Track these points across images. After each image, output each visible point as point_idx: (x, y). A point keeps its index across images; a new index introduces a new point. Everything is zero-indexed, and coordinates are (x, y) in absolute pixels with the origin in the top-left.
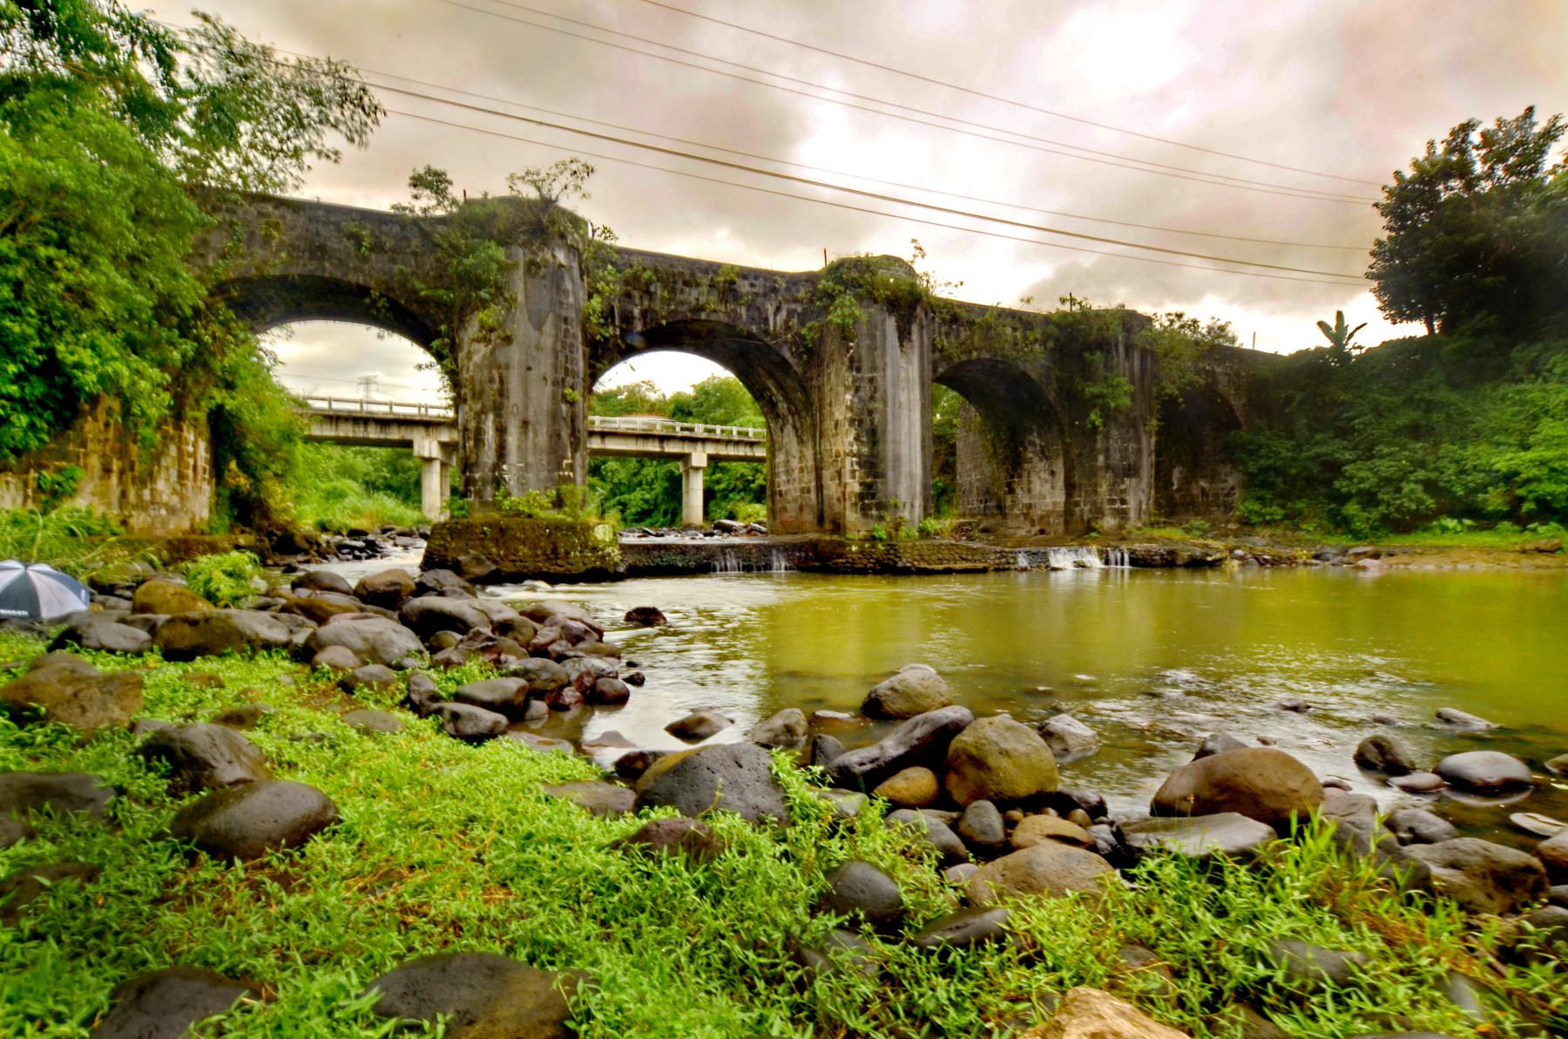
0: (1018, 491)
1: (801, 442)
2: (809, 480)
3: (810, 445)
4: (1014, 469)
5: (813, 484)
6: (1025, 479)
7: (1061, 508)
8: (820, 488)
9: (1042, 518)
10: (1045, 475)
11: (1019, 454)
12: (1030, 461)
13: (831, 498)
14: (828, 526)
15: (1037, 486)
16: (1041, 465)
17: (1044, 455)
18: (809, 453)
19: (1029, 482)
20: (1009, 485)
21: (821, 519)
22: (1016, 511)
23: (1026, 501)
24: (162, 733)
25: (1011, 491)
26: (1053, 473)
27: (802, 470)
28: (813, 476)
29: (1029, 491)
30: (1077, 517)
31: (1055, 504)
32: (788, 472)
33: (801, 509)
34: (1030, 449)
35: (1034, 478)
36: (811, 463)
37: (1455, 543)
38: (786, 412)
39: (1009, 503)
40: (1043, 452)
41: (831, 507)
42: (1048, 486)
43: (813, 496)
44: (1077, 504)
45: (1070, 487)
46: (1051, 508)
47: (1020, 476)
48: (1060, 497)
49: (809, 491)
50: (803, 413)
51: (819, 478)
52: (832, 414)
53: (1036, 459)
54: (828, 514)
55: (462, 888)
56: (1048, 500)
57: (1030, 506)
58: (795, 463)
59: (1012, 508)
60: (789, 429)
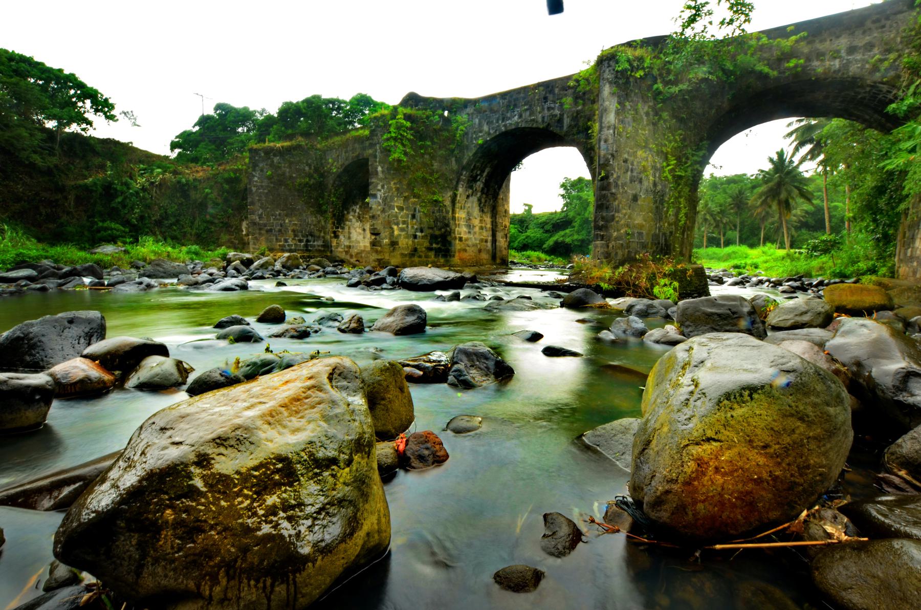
0: (341, 237)
1: (482, 211)
2: (487, 235)
4: (339, 223)
5: (490, 238)
6: (346, 230)
8: (494, 241)
9: (357, 254)
10: (360, 231)
11: (343, 215)
12: (350, 221)
13: (501, 247)
14: (498, 261)
15: (354, 236)
16: (358, 224)
17: (360, 218)
18: (488, 220)
19: (350, 233)
20: (334, 232)
21: (494, 257)
22: (340, 249)
23: (347, 243)
25: (336, 236)
26: (364, 230)
27: (481, 228)
28: (490, 233)
29: (349, 238)
33: (480, 251)
34: (352, 213)
35: (352, 231)
36: (489, 226)
38: (479, 189)
39: (334, 244)
40: (359, 217)
41: (501, 251)
42: (361, 237)
43: (489, 244)
47: (343, 228)
49: (486, 241)
50: (490, 197)
51: (494, 235)
53: (354, 220)
54: (498, 254)
55: (688, 363)
56: (362, 244)
57: (349, 247)
59: (337, 247)
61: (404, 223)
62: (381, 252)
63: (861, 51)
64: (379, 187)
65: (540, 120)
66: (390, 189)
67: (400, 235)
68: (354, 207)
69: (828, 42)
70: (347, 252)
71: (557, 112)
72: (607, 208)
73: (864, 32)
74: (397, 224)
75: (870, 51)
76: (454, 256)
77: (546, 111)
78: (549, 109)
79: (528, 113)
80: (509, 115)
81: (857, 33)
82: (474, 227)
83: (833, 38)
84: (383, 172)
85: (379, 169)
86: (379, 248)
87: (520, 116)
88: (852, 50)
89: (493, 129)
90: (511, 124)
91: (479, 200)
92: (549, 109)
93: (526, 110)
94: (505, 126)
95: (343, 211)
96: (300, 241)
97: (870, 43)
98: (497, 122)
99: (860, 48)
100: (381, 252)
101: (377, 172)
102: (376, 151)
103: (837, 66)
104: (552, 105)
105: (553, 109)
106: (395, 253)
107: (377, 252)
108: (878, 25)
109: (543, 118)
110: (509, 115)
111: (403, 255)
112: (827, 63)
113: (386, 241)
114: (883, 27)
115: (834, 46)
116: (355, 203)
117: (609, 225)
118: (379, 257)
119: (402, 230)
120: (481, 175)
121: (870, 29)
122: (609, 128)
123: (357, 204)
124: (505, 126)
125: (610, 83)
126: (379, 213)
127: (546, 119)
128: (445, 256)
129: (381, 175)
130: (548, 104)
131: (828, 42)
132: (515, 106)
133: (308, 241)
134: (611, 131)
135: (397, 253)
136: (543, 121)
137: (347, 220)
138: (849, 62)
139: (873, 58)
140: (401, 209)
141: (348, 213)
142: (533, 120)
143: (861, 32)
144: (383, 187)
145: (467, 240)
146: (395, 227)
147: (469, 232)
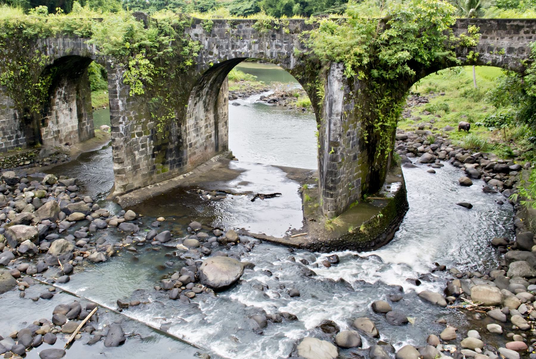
1: (207, 110)
3: (212, 111)
7: (76, 128)
10: (66, 112)
15: (62, 119)
16: (64, 106)
17: (66, 99)
18: (211, 116)
19: (57, 117)
22: (49, 137)
23: (55, 129)
24: (286, 4)
26: (71, 110)
29: (57, 122)
30: (84, 131)
31: (73, 127)
32: (197, 130)
33: (206, 148)
35: (60, 114)
37: (480, 114)
41: (222, 139)
42: (69, 118)
43: (213, 138)
44: (84, 124)
45: (80, 116)
46: (71, 130)
48: (75, 122)
52: (223, 95)
53: (60, 103)
56: (69, 126)
57: (58, 131)
58: (202, 124)
60: (201, 103)
61: (143, 146)
62: (125, 178)
63: (516, 52)
64: (121, 120)
65: (268, 54)
66: (130, 119)
67: (140, 158)
68: (60, 90)
69: (496, 40)
70: (56, 138)
71: (284, 51)
72: (336, 174)
73: (519, 39)
74: (138, 149)
75: (522, 54)
76: (186, 163)
77: (274, 48)
78: (277, 46)
79: (257, 46)
80: (238, 43)
81: (514, 38)
82: (201, 128)
83: (499, 38)
84: (123, 105)
85: (120, 103)
86: (124, 175)
87: (250, 47)
88: (510, 50)
89: (223, 53)
90: (241, 53)
91: (205, 102)
92: (277, 46)
93: (256, 43)
94: (235, 53)
95: (49, 96)
96: (10, 138)
97: (522, 47)
99: (516, 50)
100: (125, 178)
101: (118, 106)
102: (116, 86)
103: (501, 60)
104: (280, 44)
105: (281, 47)
106: (137, 176)
107: (122, 179)
108: (528, 35)
109: (272, 53)
111: (144, 175)
112: (494, 56)
113: (129, 167)
114: (531, 38)
115: (499, 45)
116: (61, 86)
117: (336, 186)
118: (124, 184)
119: (142, 153)
120: (207, 83)
121: (523, 37)
122: (337, 115)
123: (63, 85)
124: (235, 53)
125: (339, 81)
126: (122, 144)
127: (274, 55)
128: (179, 165)
129: (121, 109)
130: (276, 42)
131: (496, 40)
132: (244, 36)
133: (17, 137)
134: (339, 118)
135: (139, 175)
136: (272, 56)
137: (54, 105)
138: (508, 58)
139: (523, 59)
140: (140, 135)
141: (54, 97)
142: (262, 53)
143: (517, 38)
144: (124, 119)
145: (195, 143)
146: (136, 152)
147: (197, 135)
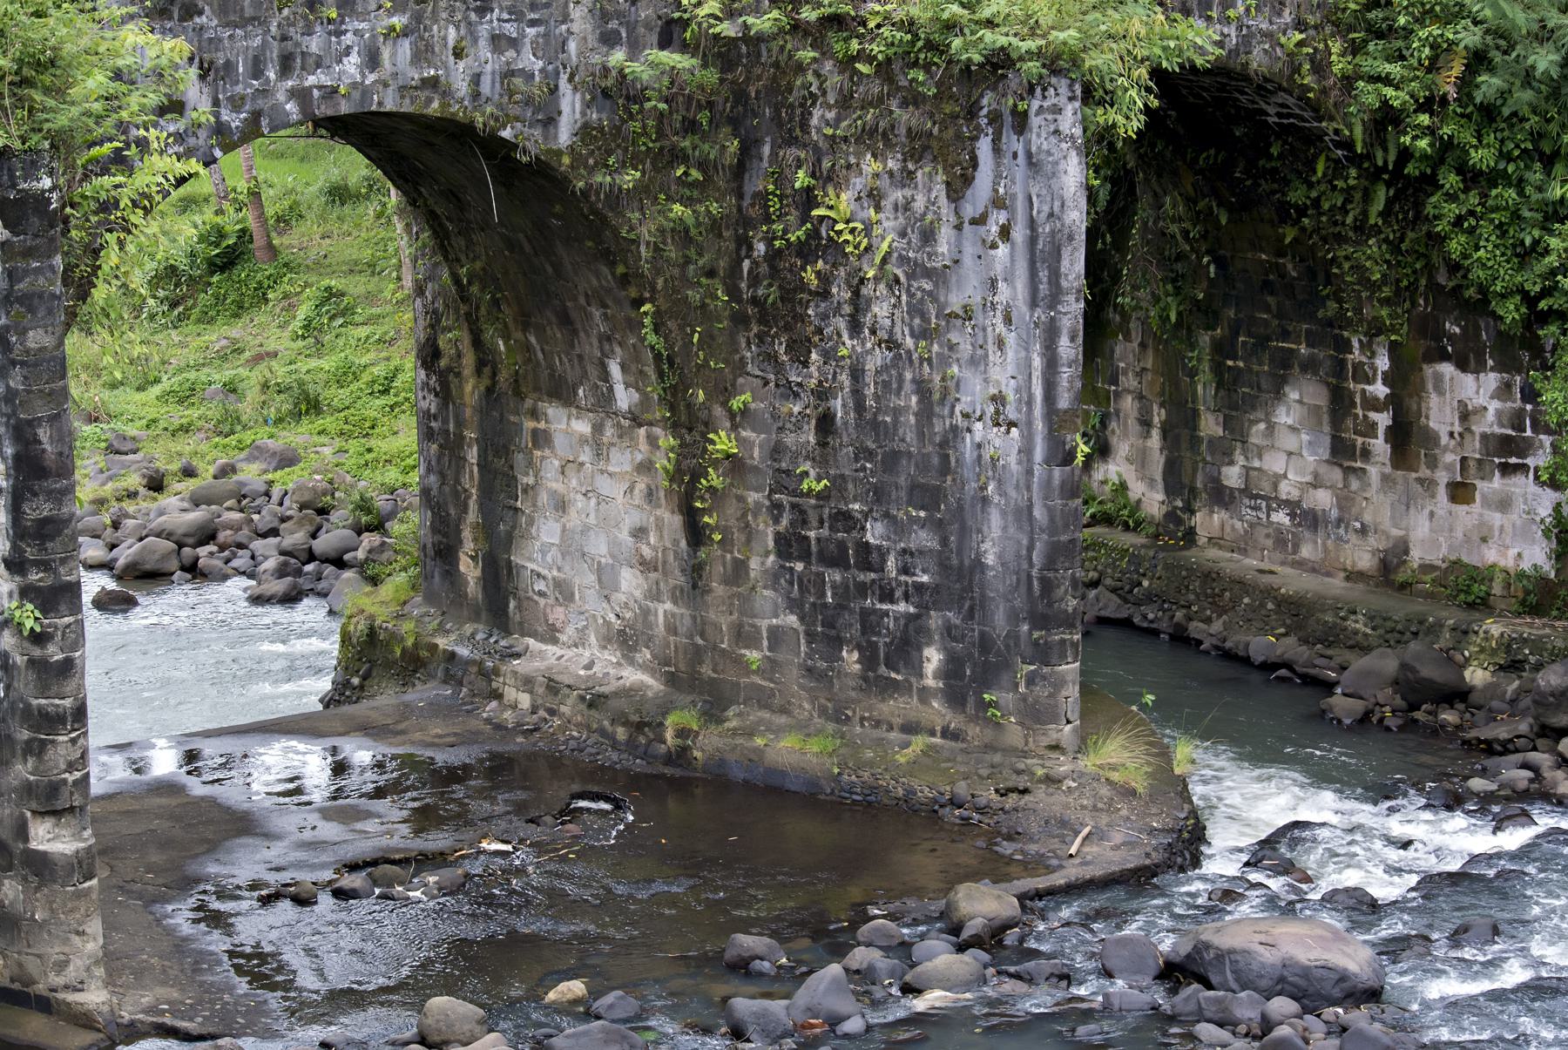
80: (314, 44)
87: (372, 60)
89: (236, 103)
98: (257, 71)
104: (510, 29)
110: (314, 44)
